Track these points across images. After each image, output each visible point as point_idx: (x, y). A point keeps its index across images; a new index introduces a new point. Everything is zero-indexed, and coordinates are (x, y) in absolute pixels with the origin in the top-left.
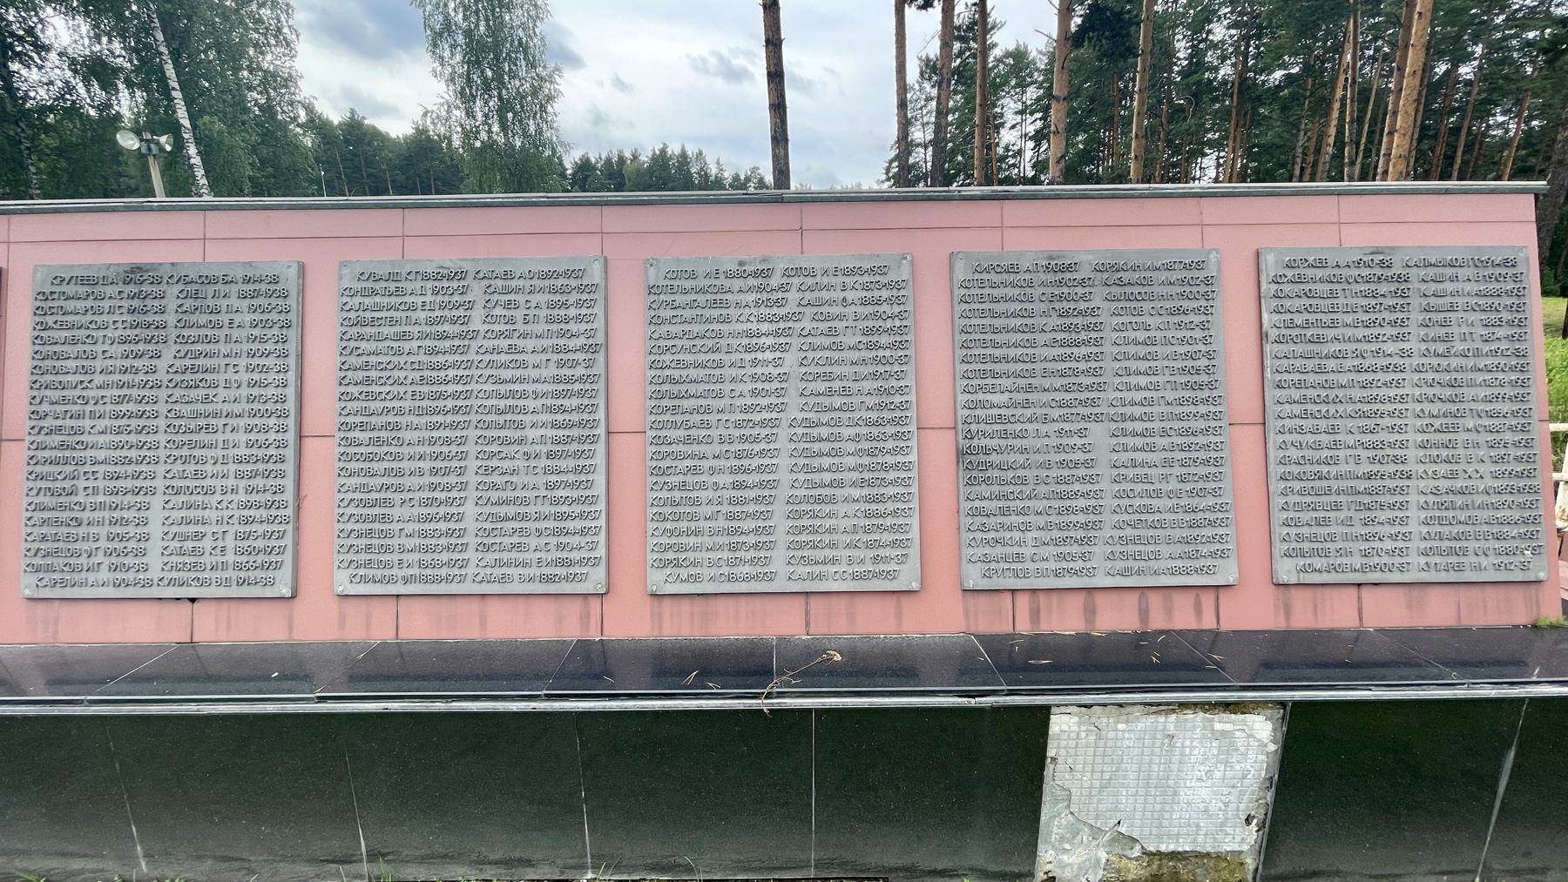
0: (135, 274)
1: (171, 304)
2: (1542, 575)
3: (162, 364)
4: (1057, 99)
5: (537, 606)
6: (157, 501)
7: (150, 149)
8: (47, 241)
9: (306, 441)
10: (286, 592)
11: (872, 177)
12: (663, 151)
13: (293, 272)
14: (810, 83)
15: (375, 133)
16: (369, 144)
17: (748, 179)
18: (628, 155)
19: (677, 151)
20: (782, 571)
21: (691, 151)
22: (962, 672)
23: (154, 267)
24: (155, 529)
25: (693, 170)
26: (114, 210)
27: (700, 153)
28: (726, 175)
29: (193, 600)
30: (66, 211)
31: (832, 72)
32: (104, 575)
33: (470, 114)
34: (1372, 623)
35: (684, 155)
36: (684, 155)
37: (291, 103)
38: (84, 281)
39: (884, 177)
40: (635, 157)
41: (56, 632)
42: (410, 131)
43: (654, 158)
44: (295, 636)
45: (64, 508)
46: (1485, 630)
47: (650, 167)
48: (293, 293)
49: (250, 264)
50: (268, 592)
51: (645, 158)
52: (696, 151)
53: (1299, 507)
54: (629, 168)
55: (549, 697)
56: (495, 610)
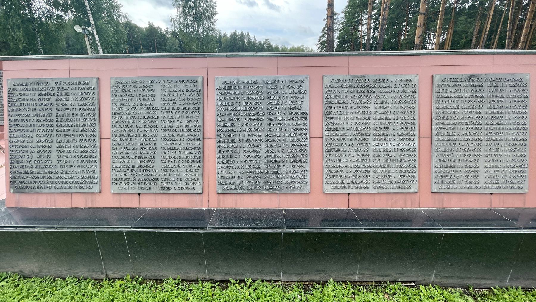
0: (471, 77)
1: (486, 89)
2: (526, 191)
3: (482, 111)
4: (421, 14)
5: (377, 197)
6: (482, 160)
7: (85, 32)
8: (19, 69)
9: (102, 140)
10: (200, 192)
11: (312, 45)
12: (235, 33)
13: (95, 81)
14: (279, 7)
15: (136, 27)
16: (134, 30)
17: (264, 44)
18: (223, 34)
19: (240, 33)
20: (462, 187)
21: (245, 33)
22: (322, 220)
23: (479, 75)
24: (481, 169)
25: (245, 40)
26: (462, 54)
27: (248, 34)
28: (257, 42)
29: (491, 194)
30: (376, 55)
31: (287, 2)
32: (464, 185)
33: (185, 19)
34: (75, 206)
35: (242, 34)
36: (242, 34)
37: (119, 16)
38: (455, 80)
39: (318, 43)
40: (225, 35)
41: (443, 204)
42: (147, 26)
43: (232, 36)
44: (210, 207)
45: (448, 161)
46: (254, 210)
47: (231, 39)
48: (418, 86)
49: (513, 74)
50: (366, 191)
51: (228, 36)
52: (247, 33)
53: (117, 166)
54: (223, 40)
55: (524, 229)
56: (364, 198)
